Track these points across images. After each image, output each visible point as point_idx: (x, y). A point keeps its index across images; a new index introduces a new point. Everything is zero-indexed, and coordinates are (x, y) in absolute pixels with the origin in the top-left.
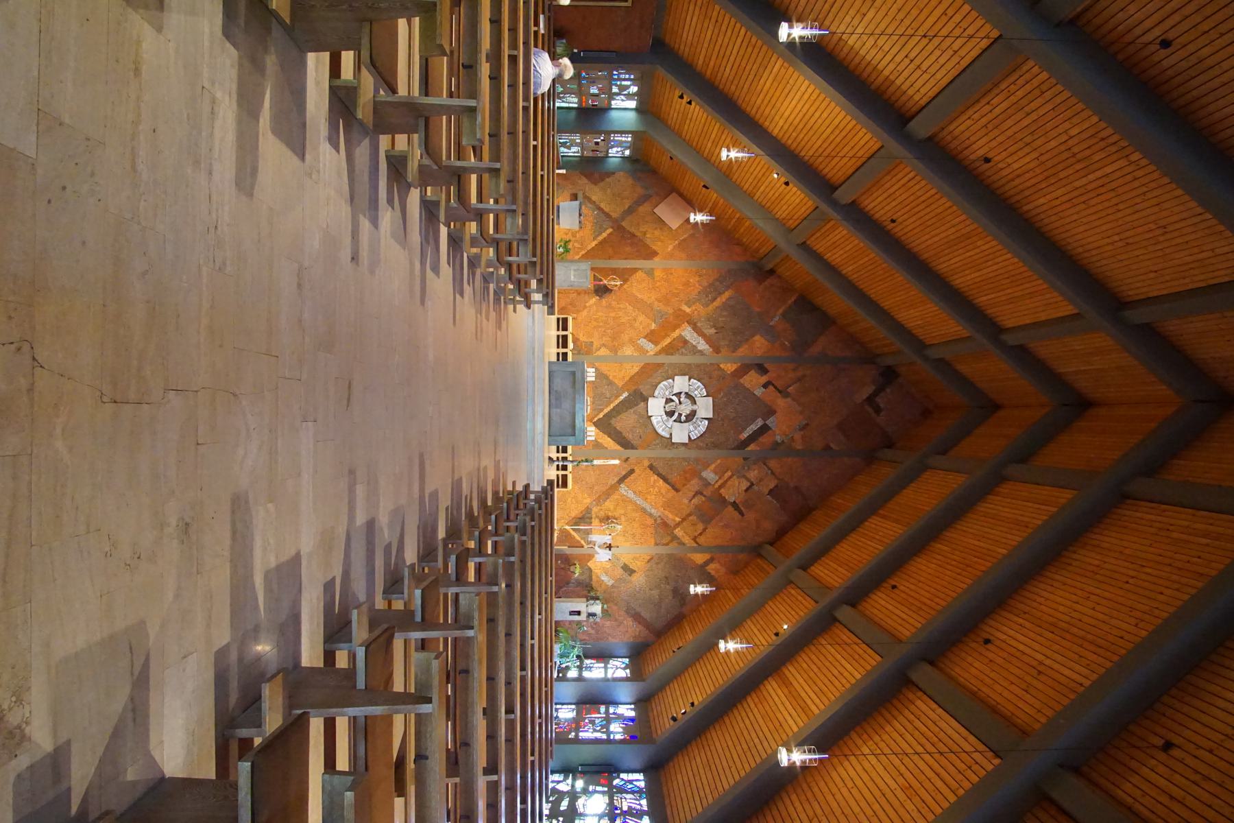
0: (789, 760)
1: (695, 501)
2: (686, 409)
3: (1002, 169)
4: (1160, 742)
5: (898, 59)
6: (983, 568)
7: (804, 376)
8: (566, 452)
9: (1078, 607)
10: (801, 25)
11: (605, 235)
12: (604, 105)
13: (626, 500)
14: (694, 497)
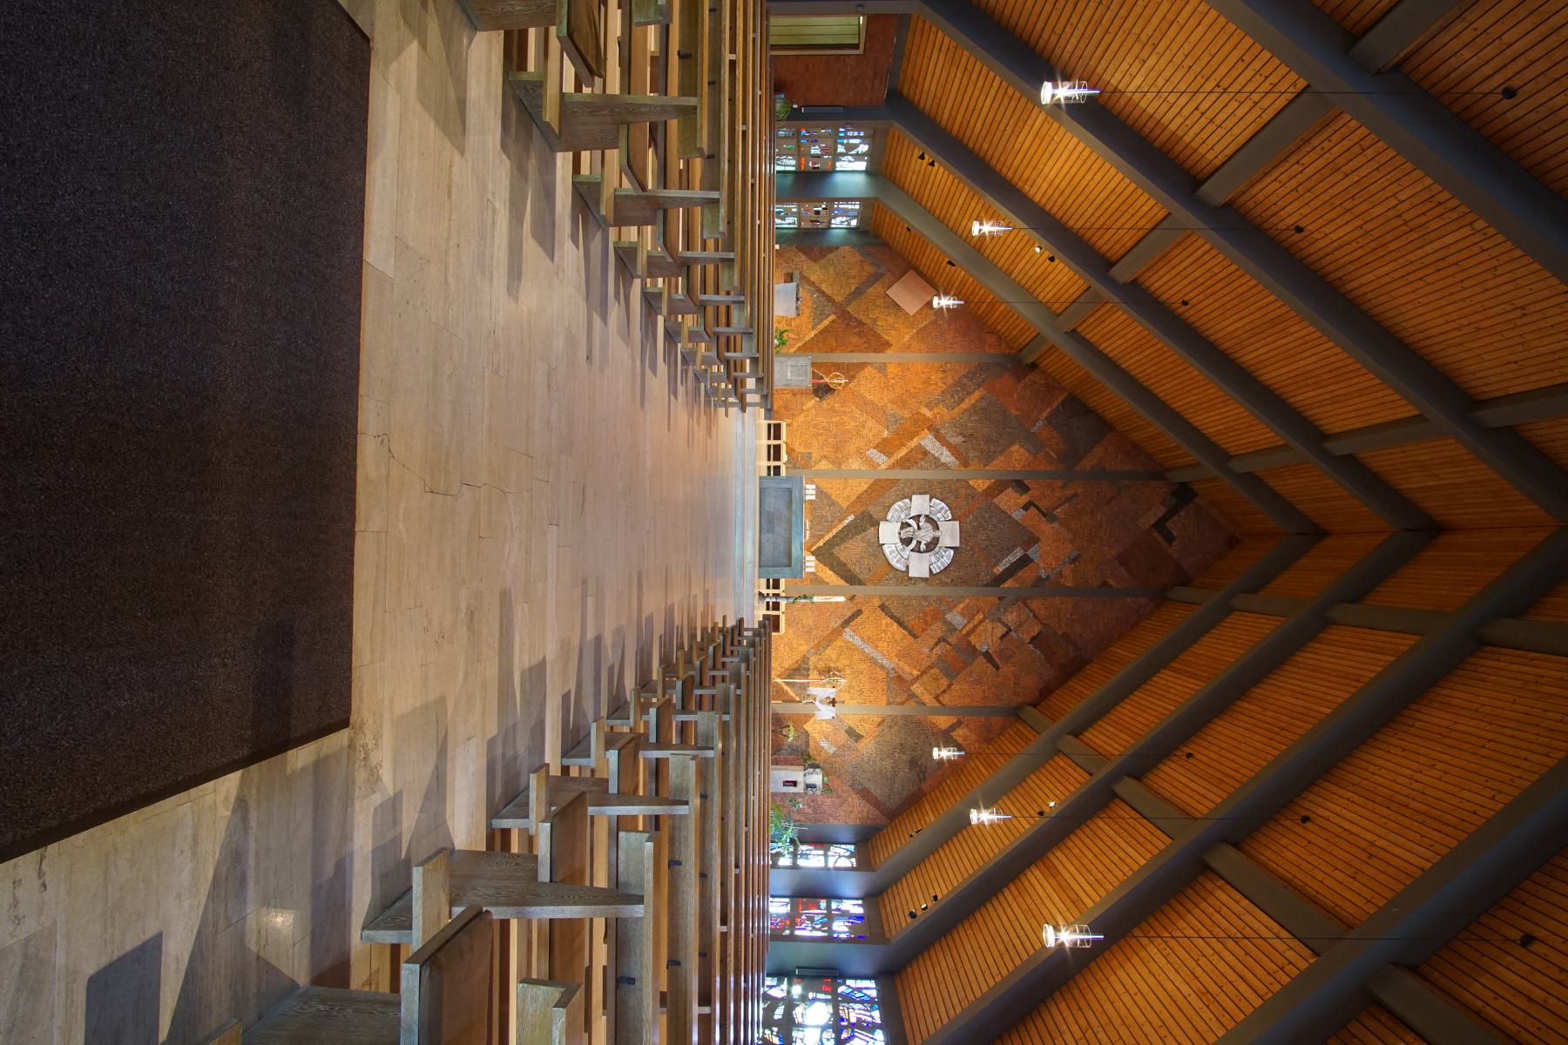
0: (1056, 940)
1: (938, 649)
2: (926, 535)
3: (1317, 240)
4: (1517, 935)
5: (1186, 112)
6: (1301, 732)
7: (1076, 494)
8: (778, 588)
9: (1418, 776)
10: (1068, 84)
11: (826, 322)
12: (828, 167)
13: (851, 648)
14: (936, 644)
